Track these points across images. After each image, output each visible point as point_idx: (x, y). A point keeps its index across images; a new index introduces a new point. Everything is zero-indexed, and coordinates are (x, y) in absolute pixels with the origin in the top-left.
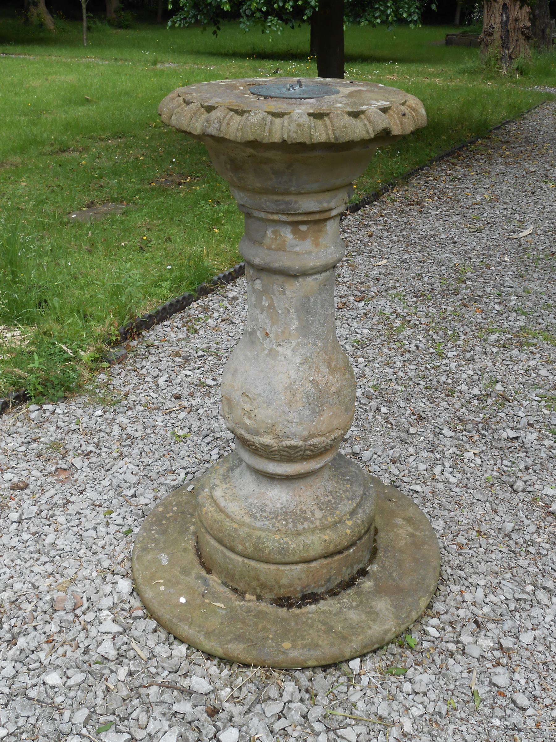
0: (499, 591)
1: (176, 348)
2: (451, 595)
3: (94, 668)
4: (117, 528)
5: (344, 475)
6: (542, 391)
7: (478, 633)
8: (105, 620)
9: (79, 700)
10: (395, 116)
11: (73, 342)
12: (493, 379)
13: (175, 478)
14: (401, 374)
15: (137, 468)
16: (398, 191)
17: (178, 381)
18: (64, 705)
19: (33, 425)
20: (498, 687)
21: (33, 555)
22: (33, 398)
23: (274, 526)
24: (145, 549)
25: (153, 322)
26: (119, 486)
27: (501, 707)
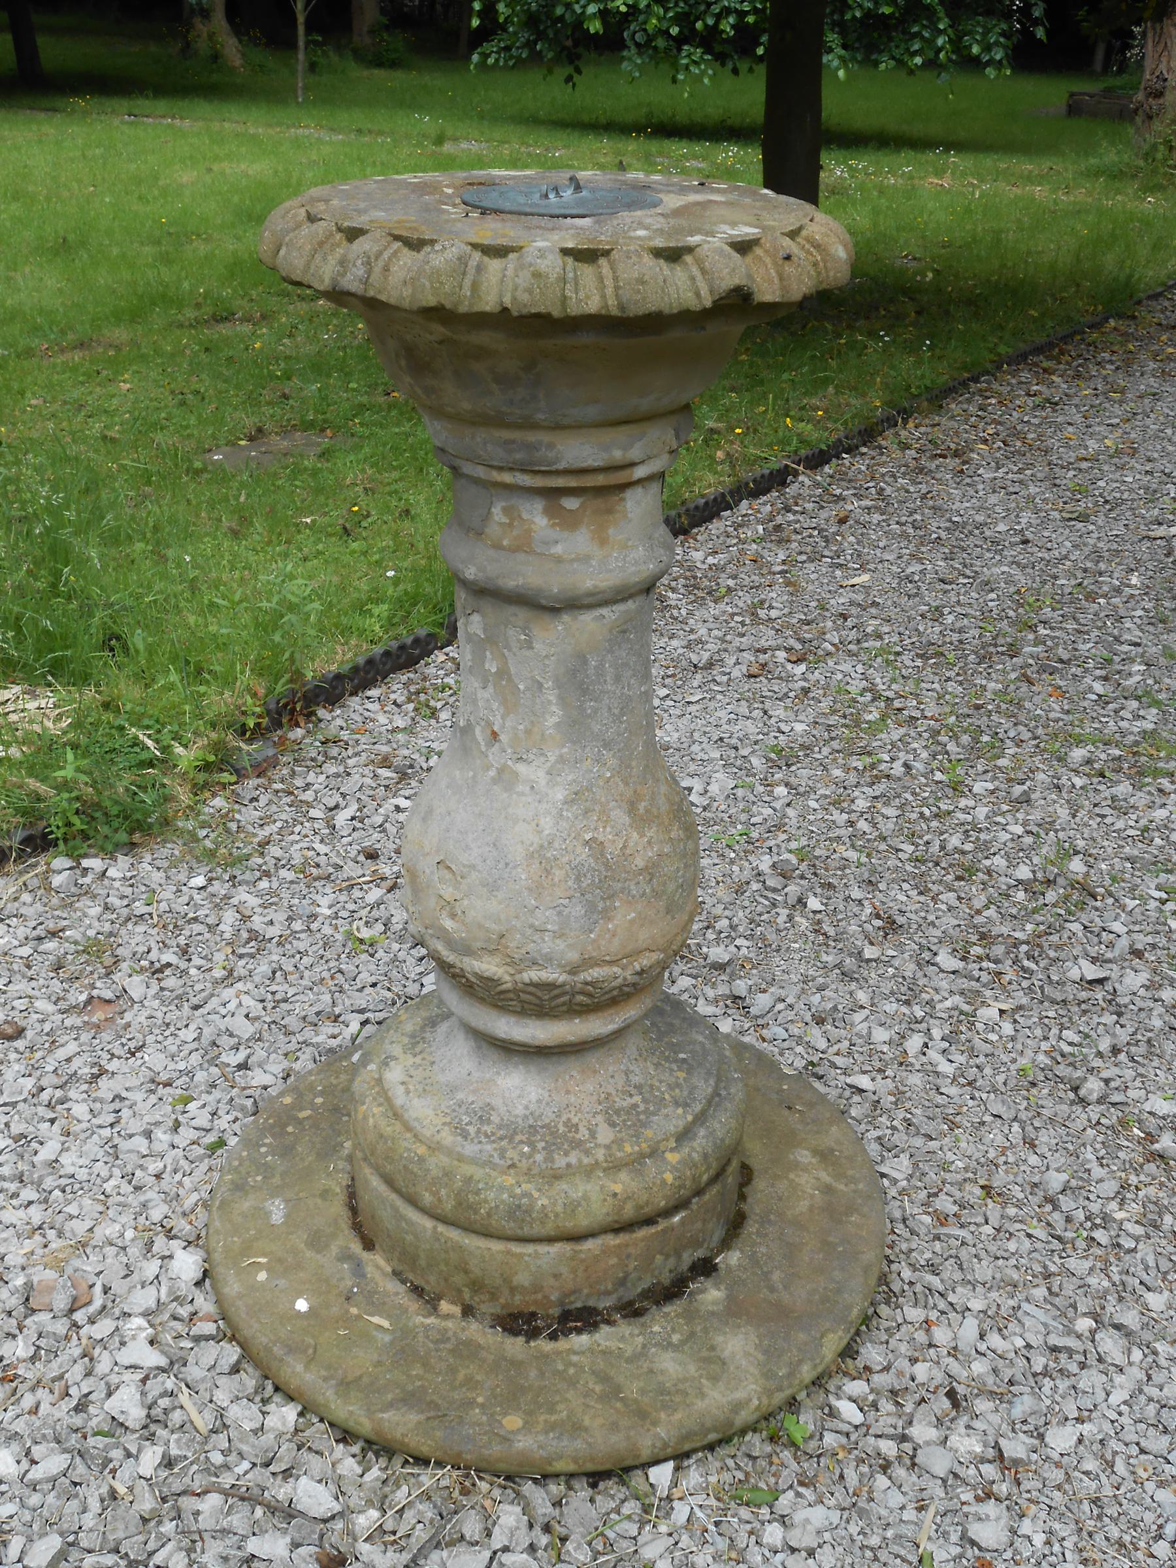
0: (1013, 1326)
1: (385, 749)
2: (903, 1329)
3: (92, 1444)
4: (193, 1135)
5: (675, 1048)
7: (952, 1420)
8: (134, 1337)
9: (45, 1513)
10: (768, 260)
11: (163, 725)
13: (336, 1031)
14: (863, 825)
15: (260, 1006)
17: (379, 820)
18: (14, 1523)
19: (55, 901)
20: (980, 1549)
22: (61, 843)
23: (502, 1157)
24: (239, 1187)
25: (344, 689)
26: (214, 1044)
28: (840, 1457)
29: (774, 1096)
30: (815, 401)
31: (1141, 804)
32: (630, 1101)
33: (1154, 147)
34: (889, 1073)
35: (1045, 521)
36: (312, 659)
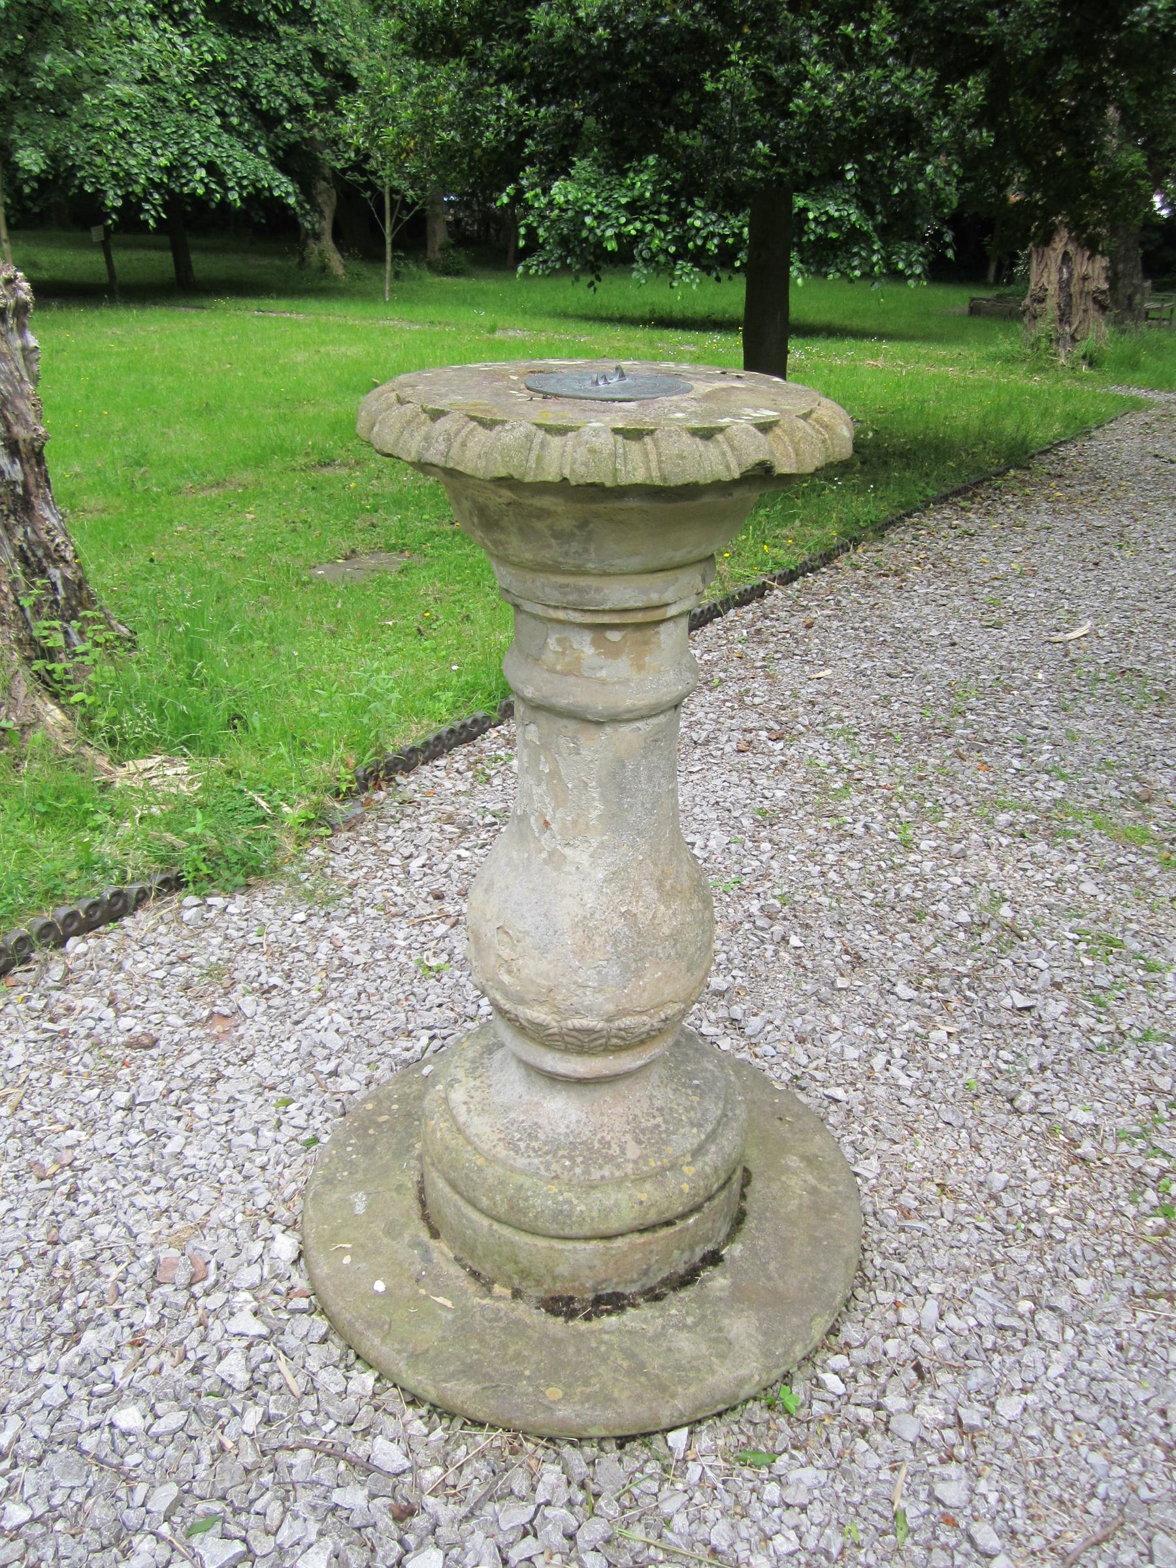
0: (966, 1308)
1: (450, 809)
2: (877, 1309)
3: (207, 1402)
4: (293, 1132)
5: (691, 1075)
6: (1082, 922)
7: (918, 1390)
8: (241, 1309)
9: (166, 1464)
10: (786, 438)
12: (997, 894)
13: (409, 1044)
14: (832, 875)
16: (865, 552)
17: (444, 867)
18: (140, 1471)
19: (185, 932)
20: (944, 1505)
21: (140, 1173)
23: (547, 1169)
24: (329, 1181)
27: (945, 1547)
29: (768, 1109)
30: (785, 532)
32: (653, 1122)
33: (1038, 339)
34: (859, 1085)
36: (392, 735)
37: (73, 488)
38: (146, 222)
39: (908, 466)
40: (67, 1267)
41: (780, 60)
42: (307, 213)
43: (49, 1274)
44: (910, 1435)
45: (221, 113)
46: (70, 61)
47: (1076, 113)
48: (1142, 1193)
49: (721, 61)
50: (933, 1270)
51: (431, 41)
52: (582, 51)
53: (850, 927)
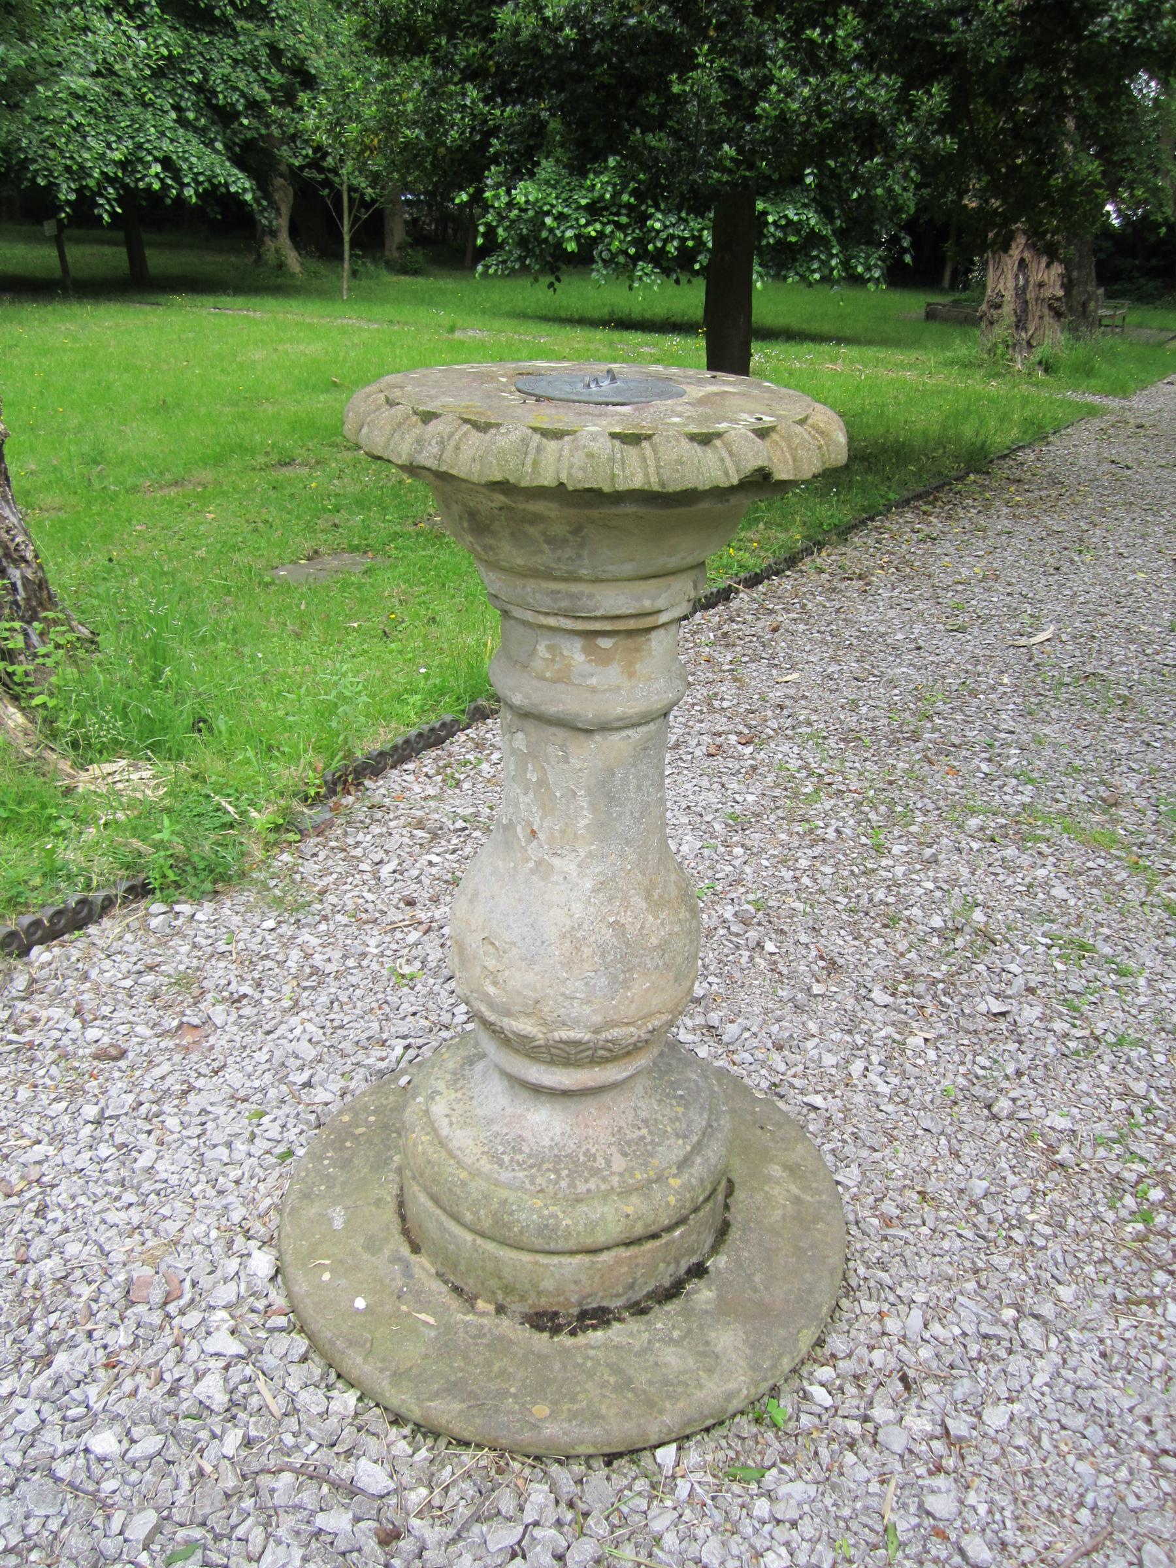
0: (950, 1316)
1: (420, 813)
2: (861, 1319)
3: (184, 1425)
4: (267, 1145)
5: (674, 1085)
7: (905, 1402)
8: (218, 1328)
11: (241, 794)
13: (384, 1054)
14: (805, 880)
16: (829, 555)
17: (415, 873)
19: (152, 940)
20: (934, 1518)
21: (110, 1189)
23: (533, 1183)
24: (306, 1196)
28: (814, 1436)
29: (749, 1117)
30: (750, 535)
31: (1025, 864)
32: (638, 1133)
33: (995, 345)
34: (838, 1093)
35: (933, 632)
37: (28, 486)
38: (100, 217)
39: (869, 470)
40: (37, 1287)
41: (745, 64)
42: (265, 209)
43: (19, 1295)
44: (898, 1448)
45: (177, 108)
46: (23, 52)
47: (1037, 121)
48: (1121, 1199)
49: (687, 64)
50: (916, 1279)
51: (394, 39)
52: (549, 51)
53: (824, 932)
